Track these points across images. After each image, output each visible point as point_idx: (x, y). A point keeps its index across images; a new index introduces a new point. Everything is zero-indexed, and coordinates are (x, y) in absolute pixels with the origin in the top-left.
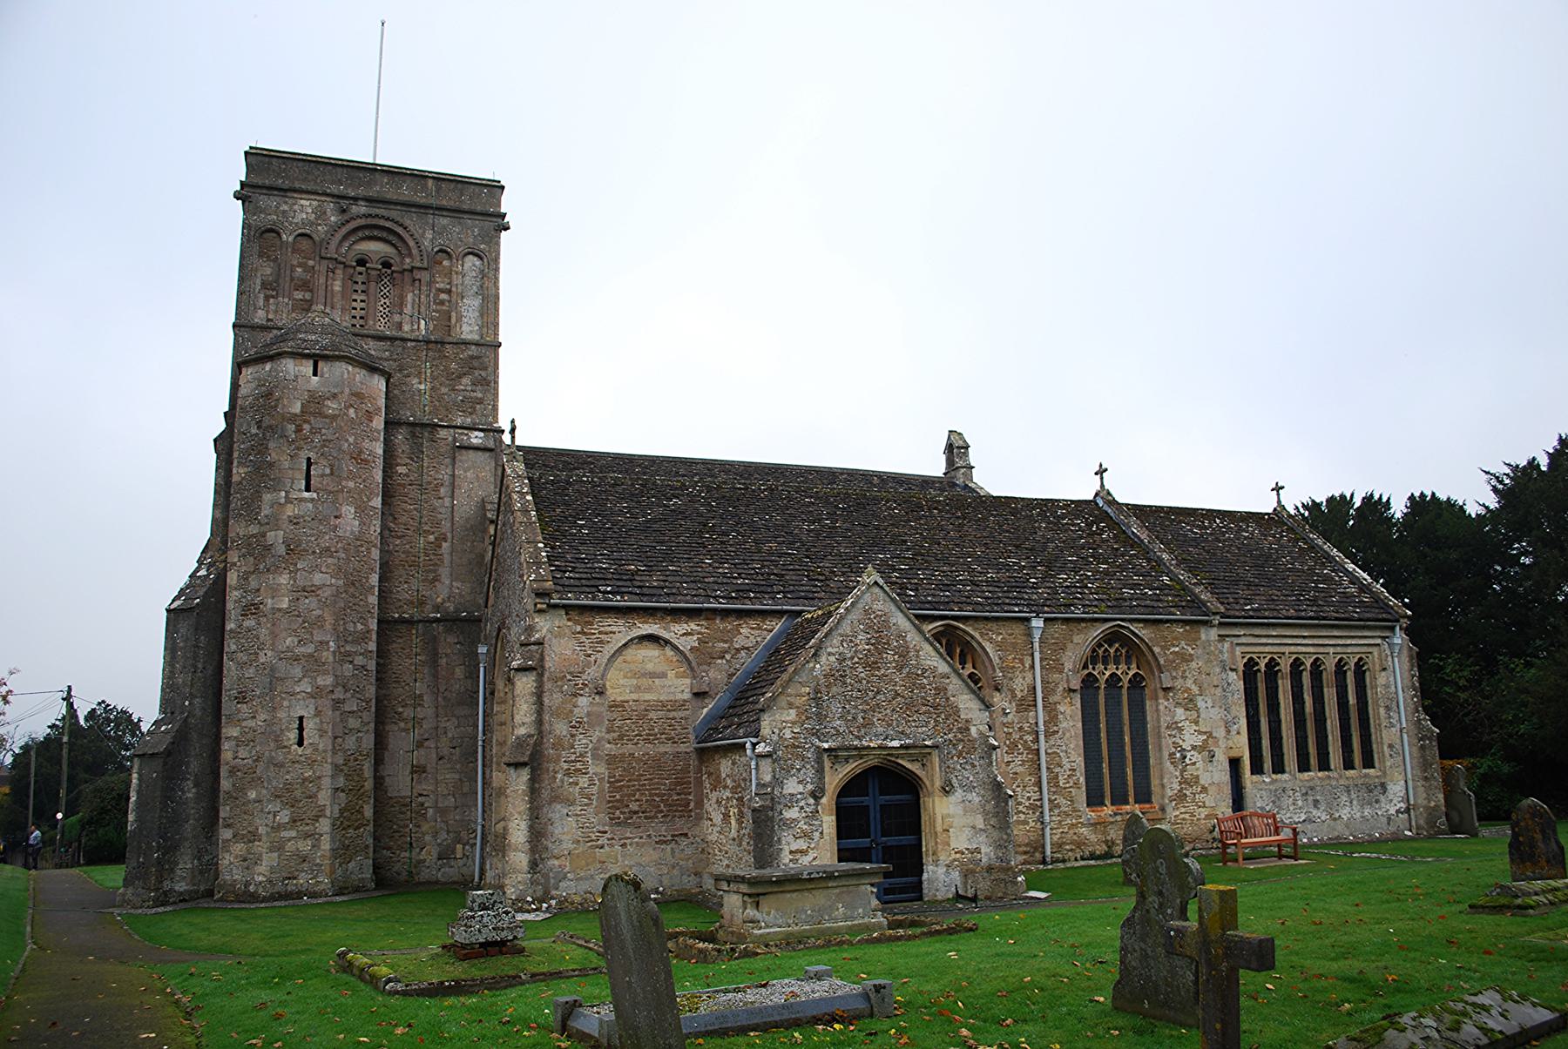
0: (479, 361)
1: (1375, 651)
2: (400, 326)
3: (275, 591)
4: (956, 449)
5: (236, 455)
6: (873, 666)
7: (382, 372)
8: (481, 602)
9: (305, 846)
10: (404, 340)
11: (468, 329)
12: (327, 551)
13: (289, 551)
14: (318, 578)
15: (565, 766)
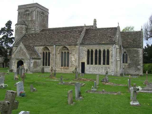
1: (110, 48)
4: (95, 21)
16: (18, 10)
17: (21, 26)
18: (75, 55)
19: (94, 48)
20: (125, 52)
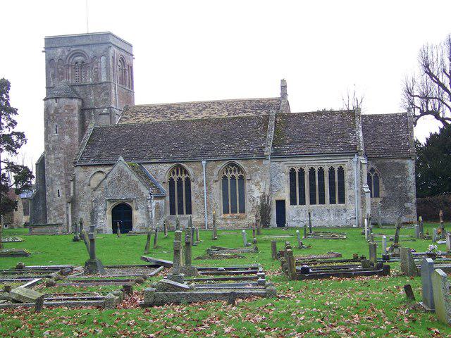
6: (119, 180)
16: (44, 50)
17: (67, 104)
18: (261, 183)
19: (307, 164)
20: (372, 170)
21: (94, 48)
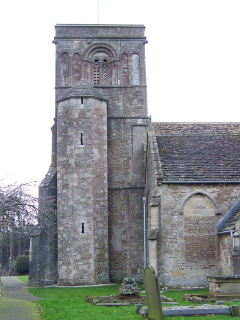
0: (139, 94)
2: (111, 82)
3: (73, 180)
5: (58, 133)
7: (105, 100)
8: (144, 181)
9: (85, 267)
10: (112, 88)
11: (135, 82)
12: (89, 166)
13: (77, 166)
14: (87, 175)
15: (170, 240)
17: (96, 106)
21: (123, 43)
